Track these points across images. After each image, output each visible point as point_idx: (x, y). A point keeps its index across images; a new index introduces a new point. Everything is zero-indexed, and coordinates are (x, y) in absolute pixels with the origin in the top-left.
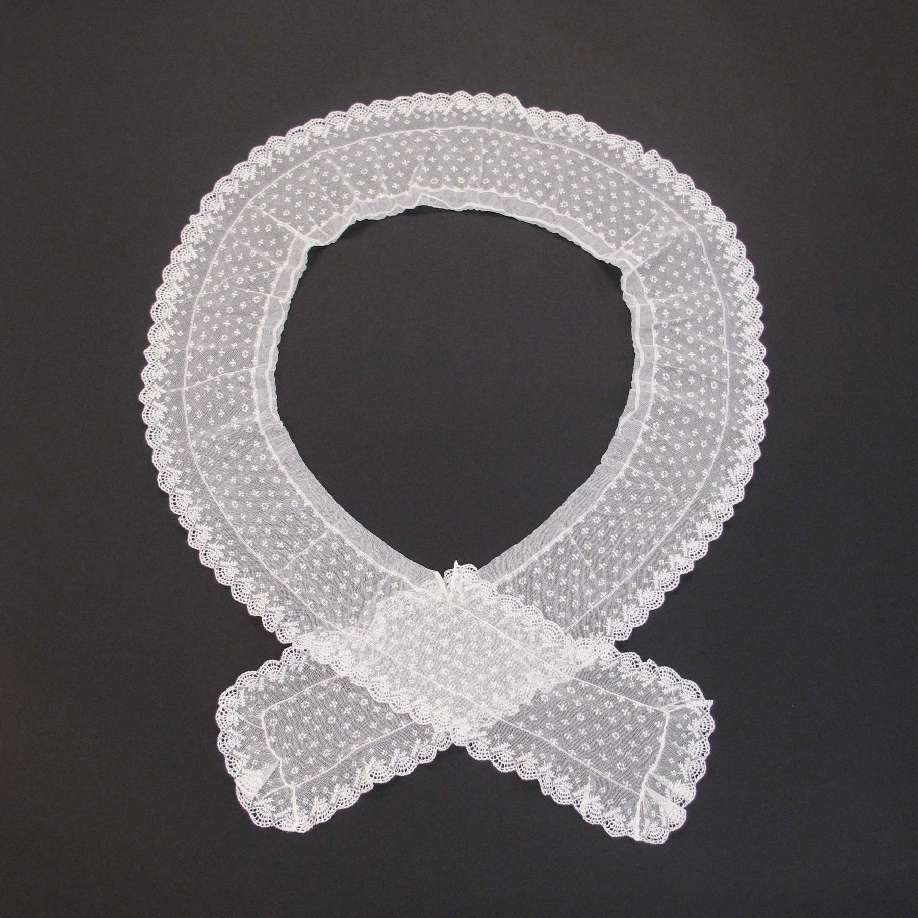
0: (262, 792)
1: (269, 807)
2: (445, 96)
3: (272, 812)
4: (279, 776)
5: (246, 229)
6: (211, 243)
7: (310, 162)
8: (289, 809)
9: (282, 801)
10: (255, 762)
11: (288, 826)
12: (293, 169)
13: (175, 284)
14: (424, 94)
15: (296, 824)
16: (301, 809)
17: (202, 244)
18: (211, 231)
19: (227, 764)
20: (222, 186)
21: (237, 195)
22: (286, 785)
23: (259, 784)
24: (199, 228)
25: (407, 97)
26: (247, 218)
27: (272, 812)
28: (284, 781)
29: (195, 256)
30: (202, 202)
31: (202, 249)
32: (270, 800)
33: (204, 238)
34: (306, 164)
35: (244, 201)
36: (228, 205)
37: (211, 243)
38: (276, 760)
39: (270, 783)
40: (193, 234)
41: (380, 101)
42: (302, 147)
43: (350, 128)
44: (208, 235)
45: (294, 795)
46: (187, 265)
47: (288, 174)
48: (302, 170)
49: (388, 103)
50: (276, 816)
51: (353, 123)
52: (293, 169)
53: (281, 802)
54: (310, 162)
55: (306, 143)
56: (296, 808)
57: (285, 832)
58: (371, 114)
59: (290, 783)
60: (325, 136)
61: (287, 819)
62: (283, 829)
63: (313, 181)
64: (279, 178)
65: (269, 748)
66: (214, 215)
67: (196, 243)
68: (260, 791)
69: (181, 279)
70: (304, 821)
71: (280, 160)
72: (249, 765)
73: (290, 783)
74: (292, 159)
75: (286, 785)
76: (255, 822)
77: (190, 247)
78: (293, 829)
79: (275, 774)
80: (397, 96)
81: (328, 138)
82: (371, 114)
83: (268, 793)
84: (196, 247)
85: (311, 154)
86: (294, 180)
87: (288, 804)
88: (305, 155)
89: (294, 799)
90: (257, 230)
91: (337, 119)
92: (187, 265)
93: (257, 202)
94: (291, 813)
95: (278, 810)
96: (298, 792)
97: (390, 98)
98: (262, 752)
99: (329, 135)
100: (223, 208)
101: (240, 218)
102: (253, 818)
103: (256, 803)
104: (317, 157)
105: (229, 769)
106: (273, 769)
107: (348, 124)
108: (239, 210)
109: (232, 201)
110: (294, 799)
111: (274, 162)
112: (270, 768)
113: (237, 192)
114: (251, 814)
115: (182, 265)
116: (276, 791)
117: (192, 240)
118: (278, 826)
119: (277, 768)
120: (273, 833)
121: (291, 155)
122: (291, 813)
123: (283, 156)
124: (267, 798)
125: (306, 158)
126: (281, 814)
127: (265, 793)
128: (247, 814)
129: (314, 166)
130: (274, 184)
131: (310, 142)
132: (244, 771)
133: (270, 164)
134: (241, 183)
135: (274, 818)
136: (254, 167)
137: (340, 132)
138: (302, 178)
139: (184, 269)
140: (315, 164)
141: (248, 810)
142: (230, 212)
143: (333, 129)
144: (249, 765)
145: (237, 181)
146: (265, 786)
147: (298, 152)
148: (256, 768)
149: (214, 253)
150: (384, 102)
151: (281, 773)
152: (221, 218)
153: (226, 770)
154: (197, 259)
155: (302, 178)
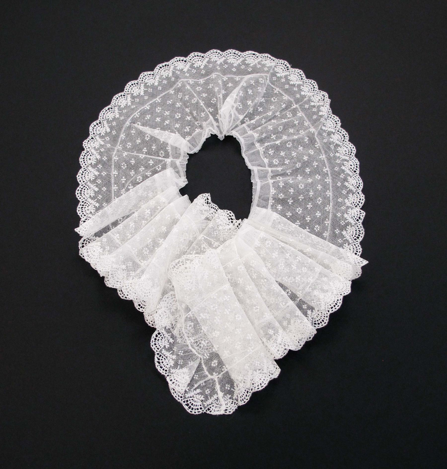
0: (191, 385)
1: (198, 396)
2: (288, 65)
3: (202, 401)
4: (202, 369)
5: (130, 144)
6: (105, 158)
7: (175, 89)
8: (215, 397)
9: (208, 390)
10: (181, 362)
11: (216, 411)
12: (161, 95)
13: (89, 200)
14: (269, 56)
15: (224, 408)
16: (225, 394)
17: (99, 162)
18: (102, 150)
19: (156, 360)
20: (106, 114)
21: (118, 119)
22: (210, 377)
23: (188, 380)
24: (93, 151)
25: (256, 53)
26: (128, 135)
27: (202, 401)
28: (207, 373)
29: (97, 173)
30: (91, 128)
31: (100, 166)
32: (198, 391)
33: (99, 157)
34: (172, 91)
35: (124, 121)
36: (111, 128)
37: (105, 158)
38: (198, 357)
39: (196, 377)
40: (89, 157)
41: (234, 51)
42: (168, 78)
43: (206, 66)
44: (101, 154)
45: (217, 383)
46: (93, 182)
47: (158, 99)
48: (168, 97)
49: (240, 53)
50: (206, 404)
51: (209, 62)
52: (161, 95)
53: (208, 392)
54: (175, 89)
55: (171, 75)
56: (220, 394)
57: (215, 416)
58: (224, 58)
59: (212, 375)
60: (185, 70)
61: (215, 405)
62: (213, 413)
63: (178, 105)
64: (151, 102)
65: (190, 348)
66: (102, 137)
67: (94, 163)
68: (189, 385)
69: (92, 195)
70: (229, 404)
71: (150, 90)
72: (176, 365)
73: (212, 375)
74: (160, 88)
75: (210, 377)
76: (189, 411)
77: (90, 168)
78: (222, 412)
79: (199, 369)
80: (248, 50)
81: (187, 72)
82: (224, 58)
83: (196, 386)
84: (94, 166)
85: (174, 83)
86: (163, 104)
87: (213, 392)
88: (171, 84)
89: (218, 387)
90: (138, 141)
91: (196, 58)
92: (93, 182)
93: (134, 121)
94: (217, 399)
95: (206, 398)
96: (221, 381)
97: (243, 50)
98: (185, 352)
99: (188, 70)
100: (108, 130)
101: (122, 136)
102: (186, 407)
103: (187, 396)
104: (179, 84)
105: (157, 364)
106: (196, 366)
107: (205, 62)
108: (120, 129)
109: (114, 124)
110: (218, 387)
111: (145, 92)
112: (194, 365)
113: (117, 116)
114: (184, 404)
115: (89, 183)
116: (202, 382)
117: (89, 162)
118: (208, 412)
119: (200, 364)
120: (205, 417)
121: (159, 85)
122: (217, 399)
123: (153, 86)
124: (195, 389)
125: (171, 86)
126: (209, 402)
127: (193, 386)
128: (181, 405)
129: (178, 92)
130: (147, 107)
131: (174, 73)
132: (172, 371)
133: (142, 93)
134: (120, 109)
135: (204, 405)
136: (129, 96)
137: (198, 68)
138: (169, 102)
139: (92, 186)
140: (178, 90)
141: (182, 402)
142: (114, 133)
143: (192, 66)
144: (176, 365)
145: (116, 108)
146: (192, 380)
147: (165, 82)
148: (182, 367)
149: (110, 166)
150: (237, 52)
151: (204, 366)
152: (108, 139)
153: (154, 364)
154: (99, 175)
155: (169, 102)
